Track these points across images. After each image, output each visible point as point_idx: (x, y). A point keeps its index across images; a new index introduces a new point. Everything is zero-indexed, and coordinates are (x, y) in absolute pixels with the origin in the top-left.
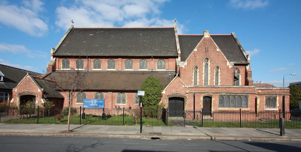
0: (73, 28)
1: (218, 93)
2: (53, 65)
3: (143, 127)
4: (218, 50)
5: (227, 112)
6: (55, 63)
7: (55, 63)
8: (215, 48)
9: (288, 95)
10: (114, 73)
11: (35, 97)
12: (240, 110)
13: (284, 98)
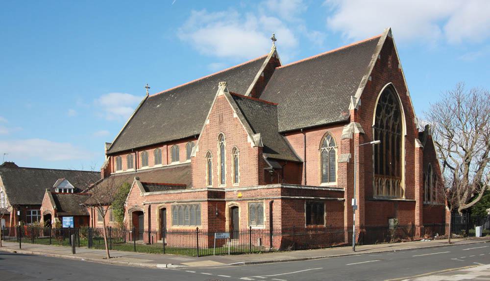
0: (148, 97)
1: (170, 203)
2: (105, 168)
3: (22, 244)
4: (235, 115)
5: (181, 232)
6: (109, 165)
7: (109, 165)
8: (232, 113)
9: (278, 199)
10: (160, 170)
11: (224, 193)
12: (197, 229)
13: (271, 204)
